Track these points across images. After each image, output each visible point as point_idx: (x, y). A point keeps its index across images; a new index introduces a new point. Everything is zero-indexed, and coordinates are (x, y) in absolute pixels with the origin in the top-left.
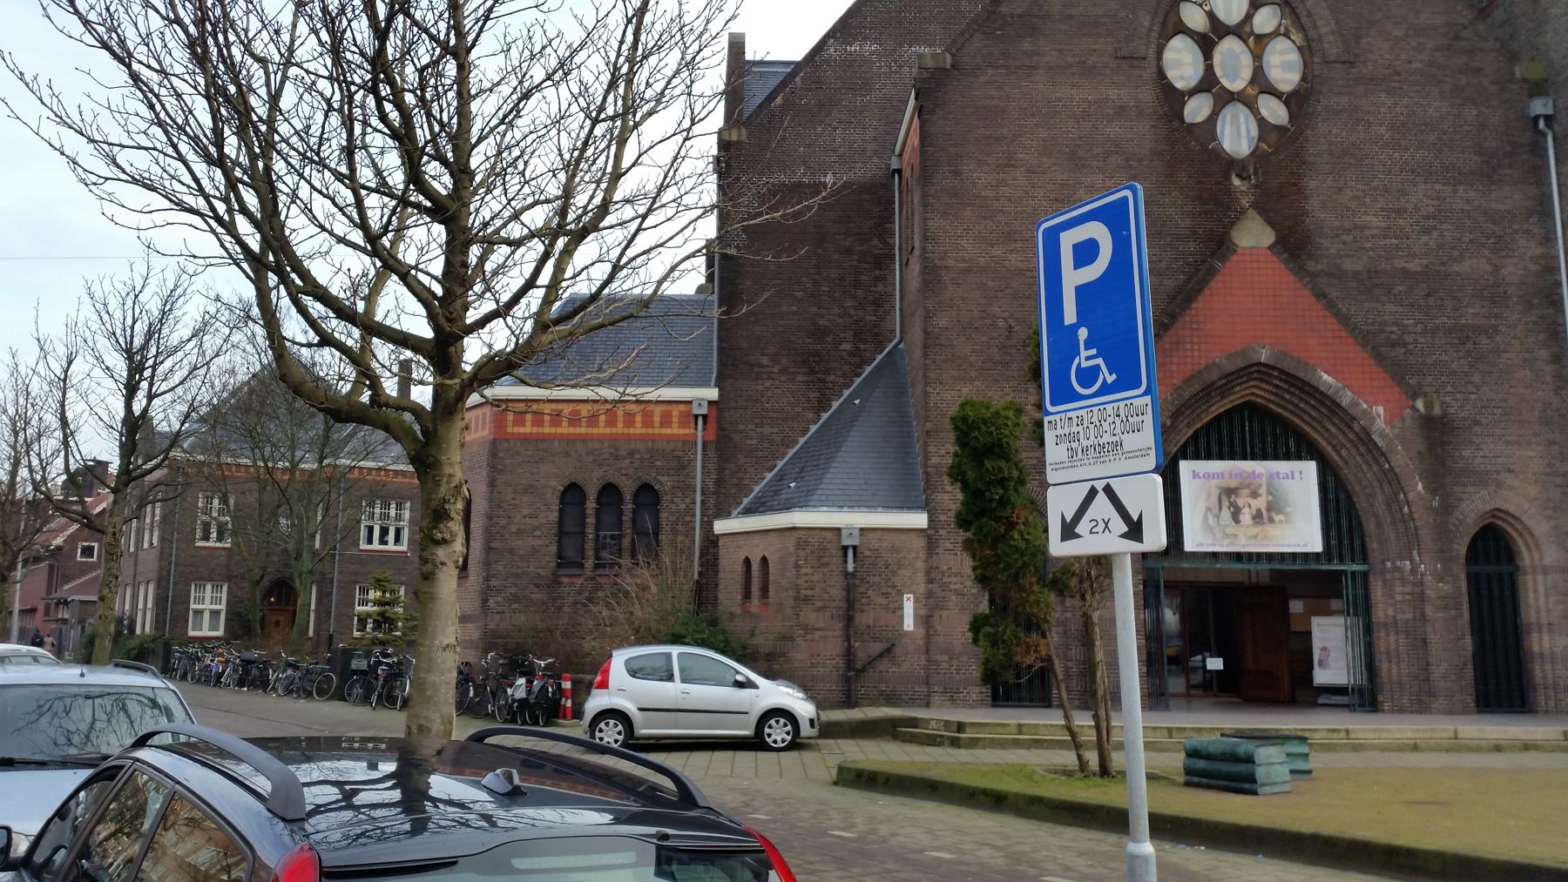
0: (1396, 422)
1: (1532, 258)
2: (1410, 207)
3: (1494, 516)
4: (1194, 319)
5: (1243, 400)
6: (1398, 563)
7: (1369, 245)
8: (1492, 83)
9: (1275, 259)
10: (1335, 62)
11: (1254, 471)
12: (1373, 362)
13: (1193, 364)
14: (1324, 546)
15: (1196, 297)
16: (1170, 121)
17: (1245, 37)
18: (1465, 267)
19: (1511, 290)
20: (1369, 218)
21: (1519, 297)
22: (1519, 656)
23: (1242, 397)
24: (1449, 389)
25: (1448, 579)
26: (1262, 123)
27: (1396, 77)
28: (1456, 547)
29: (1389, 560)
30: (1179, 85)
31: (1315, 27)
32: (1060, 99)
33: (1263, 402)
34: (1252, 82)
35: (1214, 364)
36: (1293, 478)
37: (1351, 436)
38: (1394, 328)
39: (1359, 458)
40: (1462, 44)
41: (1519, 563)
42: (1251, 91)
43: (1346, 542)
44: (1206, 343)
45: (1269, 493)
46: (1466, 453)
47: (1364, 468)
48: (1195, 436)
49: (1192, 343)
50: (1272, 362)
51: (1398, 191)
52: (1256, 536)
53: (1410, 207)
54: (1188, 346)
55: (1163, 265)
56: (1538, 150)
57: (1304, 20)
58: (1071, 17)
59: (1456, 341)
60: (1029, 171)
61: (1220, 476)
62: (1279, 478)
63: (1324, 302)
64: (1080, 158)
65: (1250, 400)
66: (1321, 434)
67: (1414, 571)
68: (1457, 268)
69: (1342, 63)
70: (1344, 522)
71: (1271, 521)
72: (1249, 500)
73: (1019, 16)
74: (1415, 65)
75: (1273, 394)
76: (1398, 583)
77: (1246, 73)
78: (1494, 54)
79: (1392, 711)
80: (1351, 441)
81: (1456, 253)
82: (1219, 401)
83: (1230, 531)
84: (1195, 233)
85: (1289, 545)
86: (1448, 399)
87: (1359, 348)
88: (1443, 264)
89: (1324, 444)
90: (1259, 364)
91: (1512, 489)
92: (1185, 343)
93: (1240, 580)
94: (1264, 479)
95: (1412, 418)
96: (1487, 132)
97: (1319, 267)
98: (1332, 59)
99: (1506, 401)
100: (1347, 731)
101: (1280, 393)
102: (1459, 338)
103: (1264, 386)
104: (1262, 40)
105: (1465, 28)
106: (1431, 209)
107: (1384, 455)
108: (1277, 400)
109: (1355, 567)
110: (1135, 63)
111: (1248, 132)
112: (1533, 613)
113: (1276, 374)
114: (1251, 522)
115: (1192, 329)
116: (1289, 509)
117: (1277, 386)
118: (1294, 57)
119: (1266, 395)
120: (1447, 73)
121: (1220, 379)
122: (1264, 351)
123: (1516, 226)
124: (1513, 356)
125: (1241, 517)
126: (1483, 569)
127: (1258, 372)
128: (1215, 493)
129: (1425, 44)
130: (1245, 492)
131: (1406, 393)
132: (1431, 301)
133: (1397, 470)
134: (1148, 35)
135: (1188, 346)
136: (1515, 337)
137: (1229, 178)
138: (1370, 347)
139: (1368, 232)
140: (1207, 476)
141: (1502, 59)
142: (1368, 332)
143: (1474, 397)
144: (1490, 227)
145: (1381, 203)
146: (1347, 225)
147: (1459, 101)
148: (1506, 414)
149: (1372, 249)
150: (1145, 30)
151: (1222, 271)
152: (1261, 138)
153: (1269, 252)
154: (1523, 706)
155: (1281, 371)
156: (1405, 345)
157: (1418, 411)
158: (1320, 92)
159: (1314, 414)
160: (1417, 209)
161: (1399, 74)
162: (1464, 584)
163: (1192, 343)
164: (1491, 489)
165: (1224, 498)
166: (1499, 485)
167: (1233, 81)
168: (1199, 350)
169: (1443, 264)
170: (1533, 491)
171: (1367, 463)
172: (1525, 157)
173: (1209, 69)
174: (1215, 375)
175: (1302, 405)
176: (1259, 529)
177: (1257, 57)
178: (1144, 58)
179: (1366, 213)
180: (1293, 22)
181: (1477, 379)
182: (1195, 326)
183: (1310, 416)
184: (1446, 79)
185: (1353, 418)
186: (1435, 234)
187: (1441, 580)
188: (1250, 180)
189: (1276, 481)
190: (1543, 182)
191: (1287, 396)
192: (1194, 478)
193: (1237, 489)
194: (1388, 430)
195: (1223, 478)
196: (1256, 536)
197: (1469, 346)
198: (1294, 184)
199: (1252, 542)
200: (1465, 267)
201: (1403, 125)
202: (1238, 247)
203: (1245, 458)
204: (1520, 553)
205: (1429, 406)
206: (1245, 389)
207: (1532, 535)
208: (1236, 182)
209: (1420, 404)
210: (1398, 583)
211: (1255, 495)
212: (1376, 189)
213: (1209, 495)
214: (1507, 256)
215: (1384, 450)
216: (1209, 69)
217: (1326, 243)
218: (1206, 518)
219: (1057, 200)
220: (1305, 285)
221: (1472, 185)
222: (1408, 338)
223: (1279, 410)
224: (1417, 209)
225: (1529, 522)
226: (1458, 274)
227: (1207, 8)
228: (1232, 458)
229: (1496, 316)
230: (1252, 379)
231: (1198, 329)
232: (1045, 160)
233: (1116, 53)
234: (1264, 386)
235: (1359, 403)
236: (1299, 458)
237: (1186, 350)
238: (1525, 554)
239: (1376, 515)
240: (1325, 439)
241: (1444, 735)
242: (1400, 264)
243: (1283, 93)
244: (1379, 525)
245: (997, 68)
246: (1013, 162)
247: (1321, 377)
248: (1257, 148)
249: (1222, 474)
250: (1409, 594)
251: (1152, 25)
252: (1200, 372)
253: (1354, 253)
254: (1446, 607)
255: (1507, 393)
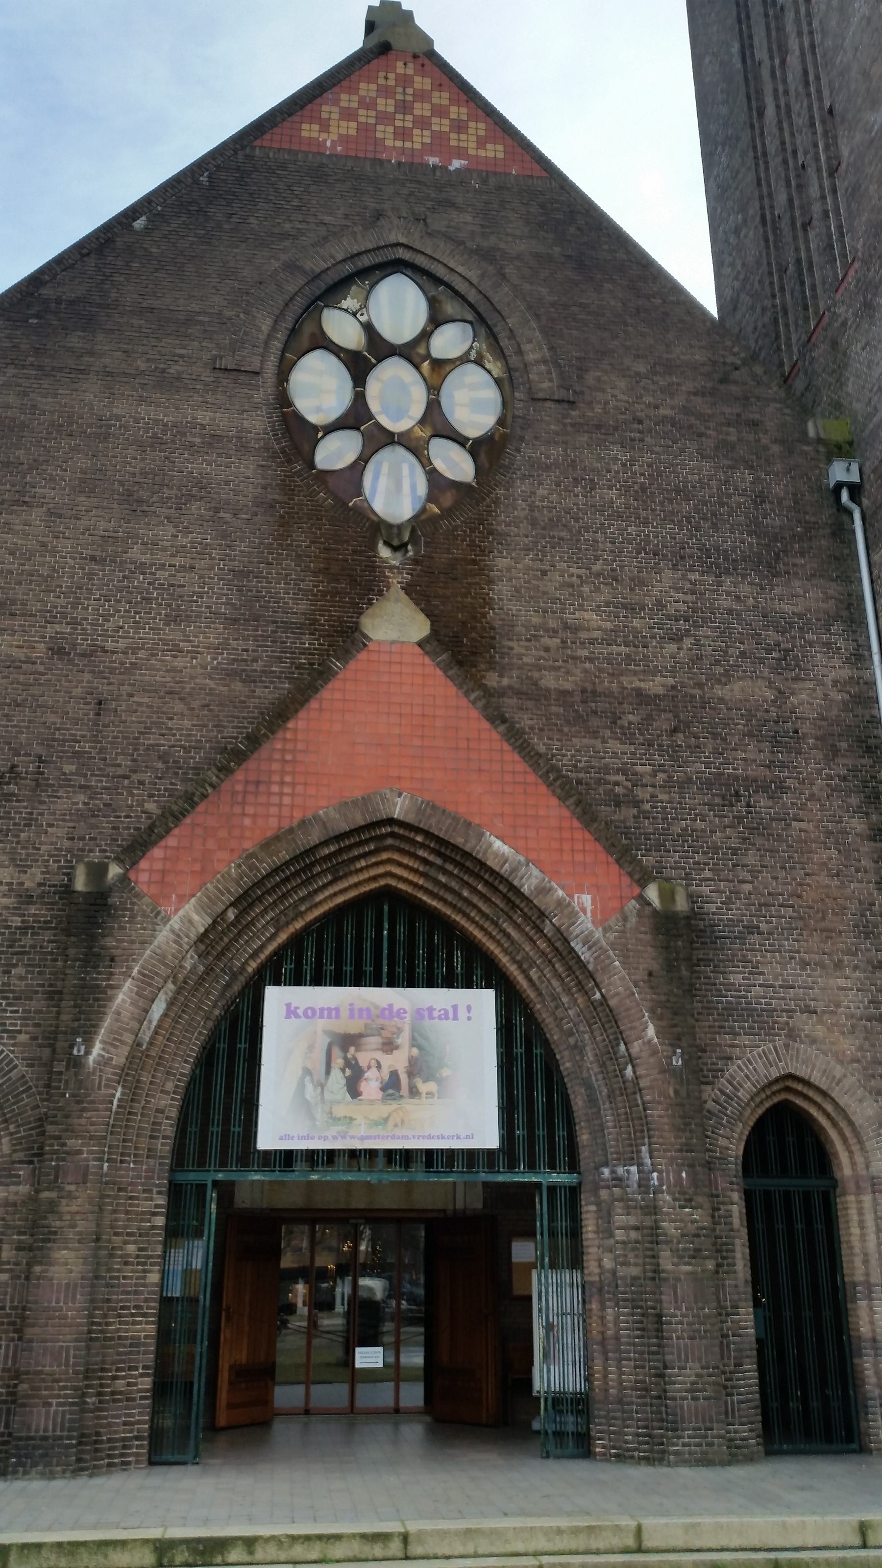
0: (612, 921)
1: (835, 683)
2: (650, 602)
3: (788, 1089)
4: (289, 746)
5: (374, 885)
6: (620, 1170)
7: (584, 653)
8: (775, 441)
9: (427, 660)
10: (546, 400)
11: (391, 1006)
12: (576, 824)
13: (280, 817)
14: (502, 1139)
15: (296, 711)
16: (289, 462)
17: (417, 360)
18: (735, 690)
19: (805, 728)
20: (586, 615)
21: (817, 739)
22: (840, 1342)
23: (374, 878)
24: (707, 874)
25: (700, 1199)
26: (432, 475)
27: (636, 426)
28: (722, 1142)
29: (606, 1164)
30: (313, 418)
31: (520, 352)
32: (118, 418)
33: (410, 890)
34: (422, 422)
35: (316, 818)
36: (455, 1018)
37: (542, 945)
38: (620, 778)
39: (555, 983)
40: (733, 388)
41: (838, 1175)
42: (419, 432)
43: (541, 1132)
44: (305, 784)
45: (414, 1043)
46: (736, 979)
47: (565, 999)
48: (297, 941)
49: (282, 783)
50: (410, 819)
51: (632, 579)
52: (386, 1120)
53: (650, 602)
54: (275, 789)
55: (258, 666)
56: (843, 534)
57: (504, 342)
58: (151, 310)
59: (717, 800)
60: (50, 513)
61: (333, 1012)
62: (431, 1018)
63: (502, 728)
64: (140, 501)
65: (387, 886)
66: (499, 943)
67: (644, 1184)
68: (719, 691)
69: (558, 401)
70: (540, 1097)
71: (414, 1092)
72: (380, 1056)
73: (71, 303)
74: (665, 411)
75: (415, 871)
76: (619, 1207)
77: (418, 410)
78: (778, 405)
79: (606, 1458)
80: (543, 954)
81: (719, 670)
82: (330, 883)
83: (340, 1111)
84: (314, 622)
85: (430, 1137)
86: (705, 890)
87: (554, 801)
88: (700, 685)
89: (504, 959)
90: (391, 821)
91: (814, 1041)
92: (270, 783)
93: (440, 1206)
94: (408, 1018)
95: (640, 915)
96: (767, 506)
97: (505, 681)
98: (541, 395)
99: (799, 897)
100: (405, 1538)
101: (432, 872)
102: (723, 797)
103: (405, 860)
104: (441, 367)
105: (736, 369)
106: (682, 607)
107: (591, 976)
108: (429, 886)
109: (556, 1178)
110: (243, 378)
111: (413, 488)
112: (858, 1262)
113: (419, 838)
114: (379, 1095)
115: (284, 761)
116: (446, 1072)
117: (425, 861)
118: (491, 395)
119: (411, 877)
120: (712, 425)
121: (325, 843)
122: (399, 800)
123: (810, 636)
124: (810, 826)
125: (363, 1086)
126: (776, 1184)
127: (392, 835)
128: (323, 1042)
129: (678, 384)
130: (374, 1041)
131: (630, 875)
132: (680, 738)
133: (612, 1003)
134: (266, 343)
135: (275, 789)
136: (812, 798)
137: (373, 548)
138: (572, 800)
139: (584, 635)
140: (311, 1013)
141: (788, 411)
142: (579, 782)
143: (747, 887)
144: (772, 636)
145: (606, 595)
146: (552, 624)
147: (728, 462)
148: (801, 918)
149: (590, 660)
150: (262, 337)
151: (340, 676)
152: (431, 497)
153: (418, 650)
154: (850, 1438)
155: (427, 834)
156: (637, 803)
157: (649, 904)
158: (522, 439)
159: (484, 908)
160: (660, 605)
161: (640, 422)
162: (737, 1210)
163: (282, 783)
164: (780, 1042)
165: (337, 1052)
166: (792, 1035)
167: (398, 418)
168: (293, 795)
169: (700, 685)
170: (848, 1046)
171: (568, 992)
172: (823, 542)
173: (360, 398)
174: (315, 837)
175: (466, 894)
176: (394, 1106)
177: (434, 389)
178: (257, 373)
179: (581, 608)
180: (490, 348)
181: (752, 859)
182: (289, 757)
183: (480, 911)
184: (708, 432)
185: (542, 915)
186: (687, 642)
187: (689, 1202)
188: (407, 551)
189: (427, 1022)
190: (850, 577)
191: (443, 879)
192: (288, 1016)
193: (361, 1036)
194: (598, 934)
195: (338, 1016)
196: (386, 1120)
197: (740, 808)
198: (474, 562)
199: (378, 1131)
200: (735, 690)
201: (643, 489)
202: (370, 640)
203: (378, 984)
204: (836, 1154)
205: (667, 896)
206: (377, 864)
207: (851, 1123)
208: (384, 552)
209: (652, 893)
210: (619, 1207)
211: (389, 1046)
212: (598, 575)
213: (311, 1048)
214: (796, 679)
215: (591, 967)
216: (360, 398)
217: (517, 648)
218: (301, 1086)
219: (93, 559)
220: (474, 703)
221: (744, 576)
222: (642, 794)
223: (434, 903)
224: (660, 605)
225: (842, 1101)
226: (721, 700)
227: (363, 319)
228: (357, 983)
229: (783, 766)
230: (386, 849)
231: (294, 761)
232: (81, 499)
233: (215, 363)
234: (405, 860)
235: (551, 889)
236: (468, 984)
237: (270, 794)
238: (843, 1156)
239: (589, 1087)
240: (505, 951)
241: (616, 1542)
242: (632, 682)
243: (468, 439)
244: (592, 1100)
245: (24, 367)
246: (27, 499)
247: (490, 845)
248: (423, 510)
249: (337, 1010)
250: (636, 1228)
251: (274, 328)
252: (291, 830)
253: (560, 663)
254: (696, 1254)
255: (801, 885)
